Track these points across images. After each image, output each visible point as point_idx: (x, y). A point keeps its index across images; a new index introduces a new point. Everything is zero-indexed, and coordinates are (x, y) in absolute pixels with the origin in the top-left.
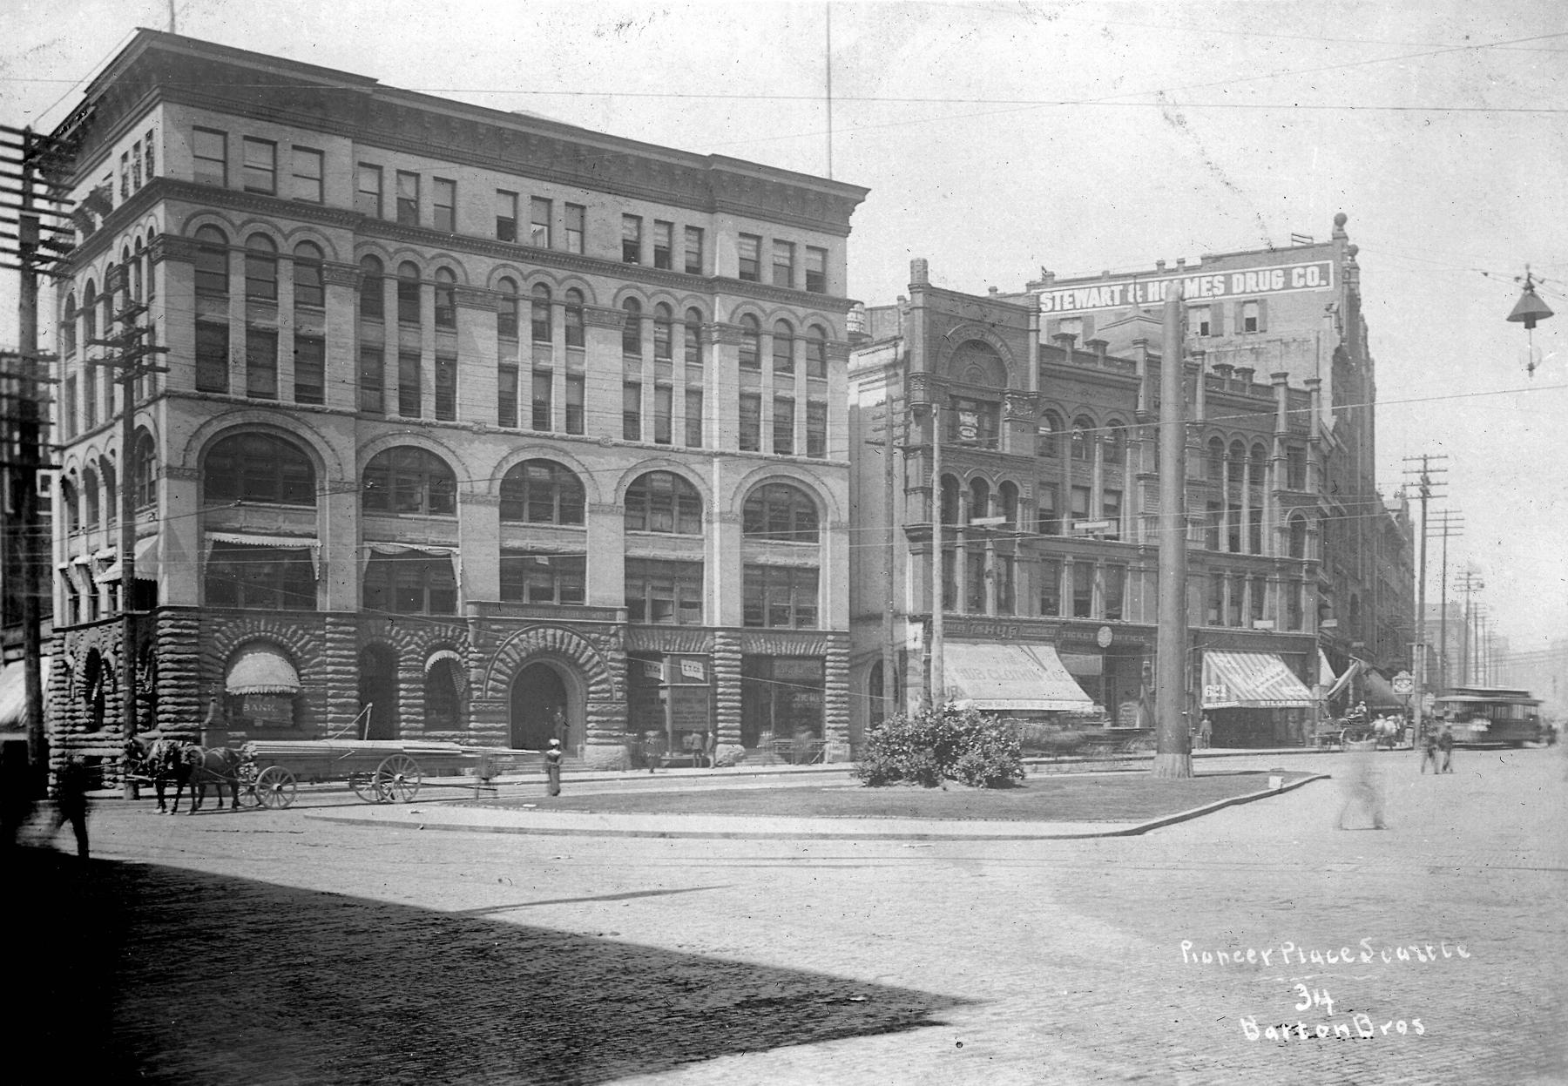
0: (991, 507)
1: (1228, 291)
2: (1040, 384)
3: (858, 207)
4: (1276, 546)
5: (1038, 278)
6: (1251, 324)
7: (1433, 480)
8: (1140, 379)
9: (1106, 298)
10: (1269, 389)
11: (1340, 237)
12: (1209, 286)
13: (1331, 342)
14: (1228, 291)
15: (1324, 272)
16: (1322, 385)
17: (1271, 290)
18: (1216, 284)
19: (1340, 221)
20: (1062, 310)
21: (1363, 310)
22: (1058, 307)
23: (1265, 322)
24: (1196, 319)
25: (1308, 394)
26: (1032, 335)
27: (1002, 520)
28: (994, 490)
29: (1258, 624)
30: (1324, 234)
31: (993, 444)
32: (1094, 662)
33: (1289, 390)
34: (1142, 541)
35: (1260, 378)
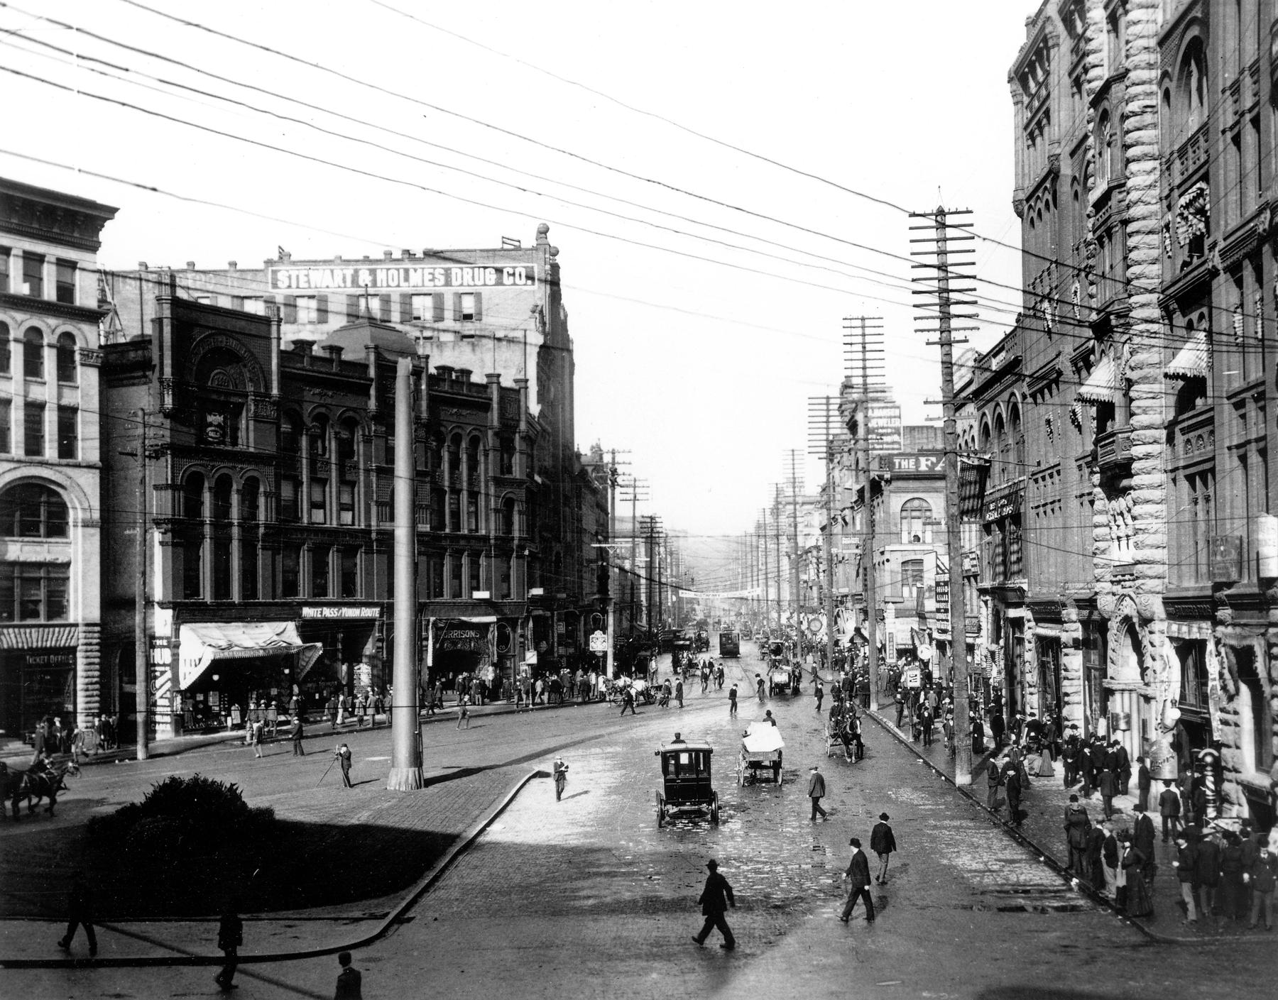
1: (448, 283)
3: (108, 224)
4: (492, 526)
5: (276, 257)
7: (619, 471)
8: (372, 380)
9: (339, 280)
10: (483, 388)
12: (431, 277)
14: (448, 283)
16: (529, 384)
17: (485, 285)
18: (436, 275)
19: (544, 232)
20: (298, 287)
22: (294, 285)
30: (529, 241)
31: (235, 443)
35: (477, 378)
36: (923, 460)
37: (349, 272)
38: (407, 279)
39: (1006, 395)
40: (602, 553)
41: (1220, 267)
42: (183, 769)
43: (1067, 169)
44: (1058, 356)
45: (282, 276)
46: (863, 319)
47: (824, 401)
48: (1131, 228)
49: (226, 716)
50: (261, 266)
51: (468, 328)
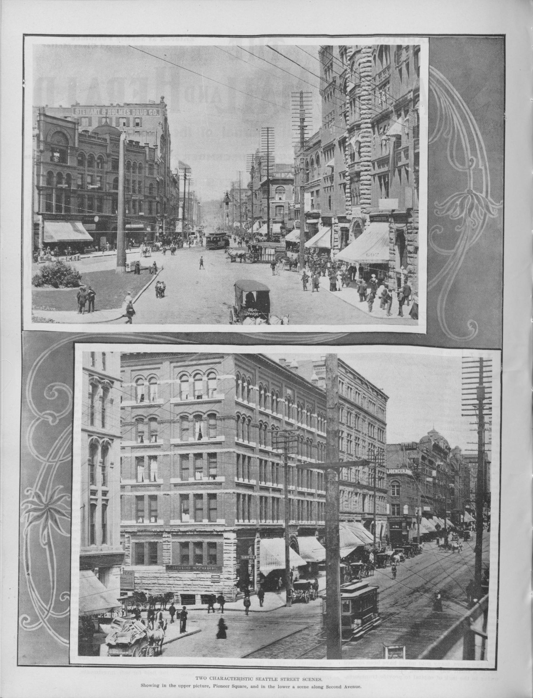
0: (64, 181)
2: (78, 145)
6: (137, 124)
10: (144, 147)
11: (162, 102)
13: (160, 133)
15: (158, 112)
19: (163, 98)
21: (168, 121)
23: (141, 123)
24: (122, 121)
25: (154, 149)
26: (76, 131)
27: (67, 186)
28: (65, 176)
29: (141, 214)
30: (158, 101)
32: (94, 226)
33: (150, 148)
34: (107, 191)
36: (283, 174)
37: (99, 110)
38: (118, 112)
39: (315, 152)
40: (324, 625)
41: (394, 110)
42: (450, 251)
43: (339, 81)
44: (334, 140)
45: (77, 110)
46: (268, 128)
47: (266, 129)
48: (362, 98)
49: (251, 261)
50: (70, 107)
51: (138, 129)
